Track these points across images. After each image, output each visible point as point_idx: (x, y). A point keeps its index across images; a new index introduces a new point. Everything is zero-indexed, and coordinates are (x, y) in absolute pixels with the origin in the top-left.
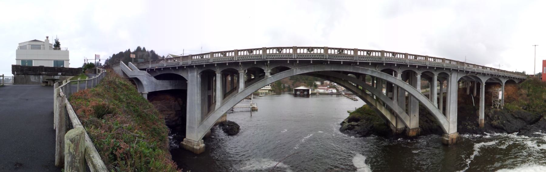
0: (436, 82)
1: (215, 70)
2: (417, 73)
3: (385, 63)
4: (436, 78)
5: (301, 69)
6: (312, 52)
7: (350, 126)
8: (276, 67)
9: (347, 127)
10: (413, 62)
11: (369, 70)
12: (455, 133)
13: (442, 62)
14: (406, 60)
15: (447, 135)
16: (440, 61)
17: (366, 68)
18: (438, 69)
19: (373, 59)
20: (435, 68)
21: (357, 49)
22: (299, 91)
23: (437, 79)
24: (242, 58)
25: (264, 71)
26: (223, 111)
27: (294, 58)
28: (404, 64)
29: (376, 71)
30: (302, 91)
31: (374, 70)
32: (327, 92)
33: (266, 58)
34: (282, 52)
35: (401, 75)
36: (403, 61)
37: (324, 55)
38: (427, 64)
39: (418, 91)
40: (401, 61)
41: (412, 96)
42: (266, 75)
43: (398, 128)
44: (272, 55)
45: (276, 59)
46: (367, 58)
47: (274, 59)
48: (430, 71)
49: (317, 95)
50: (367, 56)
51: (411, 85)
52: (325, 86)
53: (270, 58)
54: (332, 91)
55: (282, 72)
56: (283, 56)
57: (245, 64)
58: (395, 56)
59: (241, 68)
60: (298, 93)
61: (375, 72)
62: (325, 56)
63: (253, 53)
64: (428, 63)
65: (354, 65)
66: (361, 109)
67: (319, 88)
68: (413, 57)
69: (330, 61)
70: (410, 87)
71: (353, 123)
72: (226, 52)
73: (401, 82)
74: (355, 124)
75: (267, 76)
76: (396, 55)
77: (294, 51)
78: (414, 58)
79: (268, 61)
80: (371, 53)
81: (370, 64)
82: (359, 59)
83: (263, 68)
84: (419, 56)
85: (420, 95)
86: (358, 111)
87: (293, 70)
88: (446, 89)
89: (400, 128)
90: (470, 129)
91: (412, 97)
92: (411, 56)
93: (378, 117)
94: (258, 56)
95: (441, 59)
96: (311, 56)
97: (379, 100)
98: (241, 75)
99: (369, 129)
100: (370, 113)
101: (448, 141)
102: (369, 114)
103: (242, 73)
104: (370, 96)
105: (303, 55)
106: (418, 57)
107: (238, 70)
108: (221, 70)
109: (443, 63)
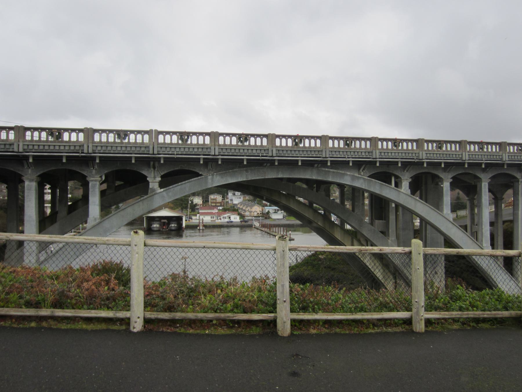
0: (486, 196)
1: (20, 173)
2: (441, 178)
3: (380, 162)
4: (485, 186)
6: (247, 144)
10: (435, 155)
11: (347, 175)
14: (421, 153)
16: (494, 150)
17: (341, 172)
18: (489, 166)
19: (356, 153)
20: (483, 166)
22: (157, 221)
23: (487, 190)
24: (104, 148)
25: (148, 179)
27: (325, 156)
28: (417, 160)
29: (360, 176)
30: (166, 221)
32: (220, 221)
33: (219, 152)
34: (189, 142)
35: (408, 183)
36: (414, 155)
37: (268, 150)
38: (464, 159)
39: (446, 216)
40: (410, 155)
41: (428, 225)
44: (171, 148)
45: (177, 154)
46: (345, 153)
47: (174, 154)
48: (471, 172)
49: (199, 230)
50: (237, 145)
51: (426, 202)
53: (166, 152)
54: (230, 218)
56: (191, 150)
57: (105, 161)
58: (399, 146)
59: (94, 171)
60: (155, 226)
61: (358, 178)
62: (270, 150)
63: (129, 139)
66: (313, 258)
68: (435, 145)
69: (279, 160)
70: (428, 208)
73: (410, 198)
75: (153, 190)
76: (400, 144)
78: (436, 146)
79: (96, 156)
80: (352, 142)
81: (351, 164)
82: (331, 156)
83: (145, 173)
84: (446, 142)
85: (450, 225)
86: (308, 263)
88: (512, 211)
91: (428, 227)
93: (352, 275)
94: (141, 147)
95: (496, 144)
96: (246, 151)
97: (359, 236)
98: (94, 186)
103: (96, 181)
105: (231, 149)
106: (444, 145)
107: (85, 173)
108: (39, 174)
109: (500, 154)
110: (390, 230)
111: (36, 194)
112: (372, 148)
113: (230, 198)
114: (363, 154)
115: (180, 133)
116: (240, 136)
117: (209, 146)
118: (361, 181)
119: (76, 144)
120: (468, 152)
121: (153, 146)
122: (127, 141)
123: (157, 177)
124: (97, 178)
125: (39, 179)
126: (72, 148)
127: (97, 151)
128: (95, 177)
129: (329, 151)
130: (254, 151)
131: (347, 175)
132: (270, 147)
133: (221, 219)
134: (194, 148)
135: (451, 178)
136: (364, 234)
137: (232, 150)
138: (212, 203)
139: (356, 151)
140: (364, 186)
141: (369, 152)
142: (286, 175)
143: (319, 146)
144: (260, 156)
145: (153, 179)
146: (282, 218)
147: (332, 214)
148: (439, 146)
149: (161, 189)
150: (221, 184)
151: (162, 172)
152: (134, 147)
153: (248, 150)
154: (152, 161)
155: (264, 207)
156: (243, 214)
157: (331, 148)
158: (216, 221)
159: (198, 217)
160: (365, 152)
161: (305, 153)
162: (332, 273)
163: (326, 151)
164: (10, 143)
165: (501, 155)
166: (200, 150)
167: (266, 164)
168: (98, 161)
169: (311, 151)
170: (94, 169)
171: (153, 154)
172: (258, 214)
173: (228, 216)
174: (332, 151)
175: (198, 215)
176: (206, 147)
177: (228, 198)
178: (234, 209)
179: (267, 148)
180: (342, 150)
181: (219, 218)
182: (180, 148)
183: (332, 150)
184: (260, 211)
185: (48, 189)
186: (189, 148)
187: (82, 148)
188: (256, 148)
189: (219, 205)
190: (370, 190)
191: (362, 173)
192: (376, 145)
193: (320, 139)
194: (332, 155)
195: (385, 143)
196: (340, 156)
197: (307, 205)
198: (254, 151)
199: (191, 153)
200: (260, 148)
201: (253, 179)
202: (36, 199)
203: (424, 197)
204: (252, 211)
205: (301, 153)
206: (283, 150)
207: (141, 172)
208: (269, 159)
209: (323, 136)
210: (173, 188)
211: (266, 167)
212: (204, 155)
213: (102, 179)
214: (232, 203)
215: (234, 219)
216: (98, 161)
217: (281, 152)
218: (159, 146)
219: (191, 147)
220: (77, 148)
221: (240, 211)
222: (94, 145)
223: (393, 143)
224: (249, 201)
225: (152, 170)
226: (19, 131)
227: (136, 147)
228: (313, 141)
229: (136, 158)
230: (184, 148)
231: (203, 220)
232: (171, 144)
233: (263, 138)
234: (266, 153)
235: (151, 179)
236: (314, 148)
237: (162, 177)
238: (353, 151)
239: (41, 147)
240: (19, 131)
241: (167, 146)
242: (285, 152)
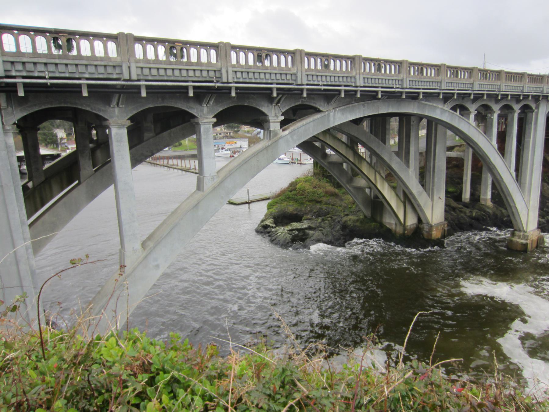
1: (101, 114)
7: (296, 232)
8: (293, 105)
9: (291, 234)
11: (438, 107)
12: (534, 230)
13: (290, 65)
15: (522, 233)
21: (229, 44)
26: (157, 266)
43: (408, 226)
47: (44, 78)
50: (168, 62)
72: (327, 57)
82: (235, 80)
83: (264, 109)
89: (410, 225)
90: (544, 223)
95: (347, 58)
100: (319, 200)
101: (526, 245)
102: (317, 202)
103: (209, 123)
104: (367, 162)
115: (169, 41)
116: (172, 45)
120: (306, 70)
122: (74, 53)
135: (214, 117)
139: (288, 72)
144: (215, 81)
148: (325, 64)
151: (283, 109)
162: (318, 206)
164: (115, 65)
165: (354, 77)
171: (130, 80)
192: (228, 58)
193: (115, 40)
195: (242, 55)
197: (343, 142)
203: (373, 132)
207: (260, 109)
211: (381, 100)
212: (277, 84)
223: (256, 54)
226: (127, 43)
228: (150, 48)
234: (117, 74)
240: (127, 43)
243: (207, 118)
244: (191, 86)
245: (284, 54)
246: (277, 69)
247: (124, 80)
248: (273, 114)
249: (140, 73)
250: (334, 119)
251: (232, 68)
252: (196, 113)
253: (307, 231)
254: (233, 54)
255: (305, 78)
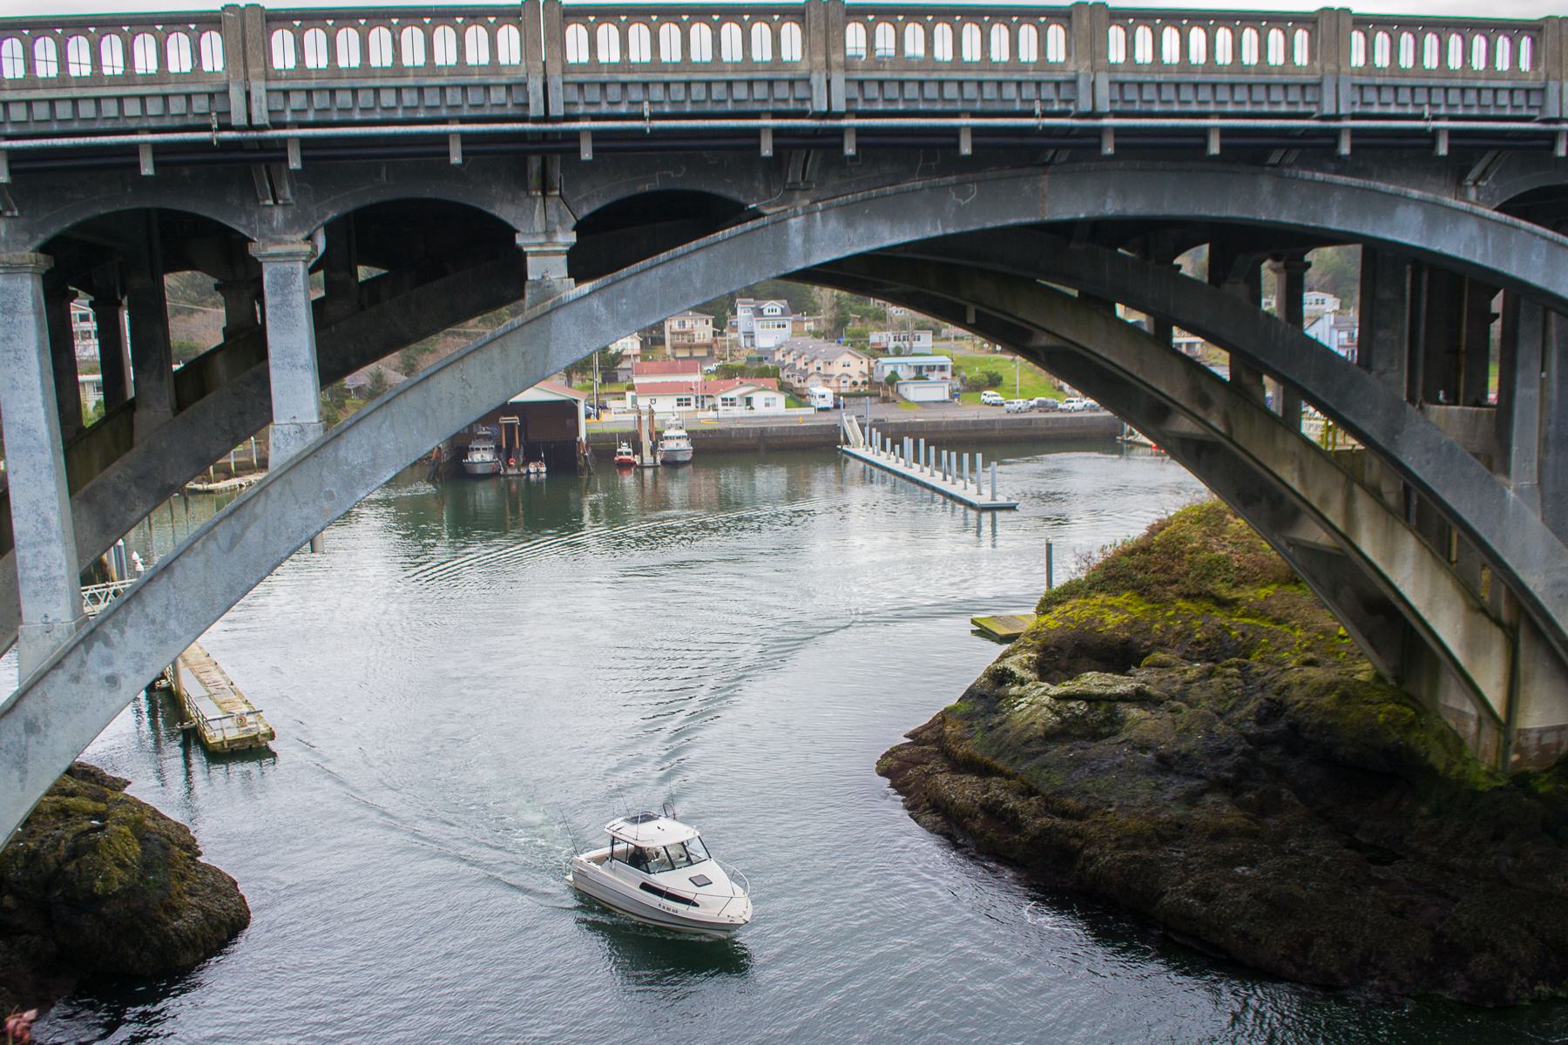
5: (850, 214)
7: (1081, 707)
9: (1057, 713)
11: (1407, 199)
13: (1525, 64)
19: (1471, 97)
21: (1347, 11)
24: (320, 101)
25: (519, 240)
29: (1463, 205)
31: (1449, 201)
33: (848, 101)
37: (1073, 82)
42: (532, 276)
44: (624, 85)
45: (654, 117)
46: (1421, 97)
47: (640, 117)
52: (690, 364)
53: (604, 108)
54: (749, 401)
55: (680, 250)
59: (278, 215)
60: (476, 457)
62: (1082, 84)
64: (1104, 92)
65: (1292, 157)
66: (1140, 558)
67: (637, 380)
71: (1093, 681)
74: (1120, 689)
77: (818, 39)
79: (285, 140)
83: (505, 212)
87: (780, 222)
89: (1543, 732)
92: (1197, 36)
93: (1304, 627)
94: (487, 87)
98: (286, 281)
99: (1252, 728)
105: (902, 83)
107: (239, 225)
108: (41, 239)
110: (1514, 449)
111: (40, 328)
112: (1541, 69)
113: (742, 328)
114: (1503, 99)
117: (802, 71)
118: (1470, 228)
119: (192, 88)
121: (545, 77)
123: (558, 228)
124: (293, 242)
125: (45, 262)
126: (177, 106)
127: (289, 117)
128: (286, 243)
129: (1353, 85)
130: (1010, 92)
131: (1407, 199)
132: (1081, 71)
133: (715, 408)
134: (730, 83)
136: (1407, 464)
137: (908, 87)
138: (674, 347)
139: (1471, 83)
140: (1479, 252)
141: (1528, 91)
142: (1136, 206)
143: (1305, 63)
144: (647, 114)
145: (542, 239)
146: (947, 397)
147: (1266, 379)
149: (579, 281)
150: (849, 252)
152: (456, 86)
153: (980, 83)
154: (535, 152)
155: (874, 357)
156: (798, 385)
157: (1360, 72)
158: (700, 415)
159: (628, 403)
160: (1512, 91)
161: (1241, 94)
163: (1337, 86)
166: (760, 91)
167: (1051, 153)
168: (295, 164)
169: (1268, 86)
170: (276, 202)
171: (547, 118)
172: (855, 384)
173: (741, 396)
174: (1361, 87)
175: (629, 394)
176: (786, 75)
177: (735, 328)
178: (761, 369)
179: (1070, 75)
180: (1408, 82)
181: (708, 402)
182: (667, 84)
183: (1364, 80)
184: (864, 375)
185: (80, 307)
186: (709, 84)
187: (219, 105)
188: (1017, 77)
189: (703, 353)
190: (1506, 271)
191: (1472, 194)
192: (1097, 47)
193: (1310, 26)
194: (1363, 104)
196: (1400, 110)
198: (1010, 92)
199: (719, 108)
200: (1038, 76)
201: (989, 225)
202: (40, 351)
204: (831, 376)
205: (1223, 94)
206: (1140, 85)
208: (1071, 128)
209: (1323, 11)
210: (634, 278)
211: (1050, 169)
212: (776, 115)
213: (315, 248)
214: (753, 345)
215: (767, 405)
216: (295, 164)
217: (1131, 94)
218: (569, 78)
219: (720, 77)
220: (200, 105)
221: (783, 375)
222: (274, 85)
224: (816, 335)
225: (534, 198)
227: (464, 88)
228: (971, 33)
229: (466, 138)
230: (688, 84)
231: (652, 413)
232: (625, 65)
233: (1047, 25)
235: (532, 241)
236: (1281, 70)
237: (579, 228)
238: (1459, 83)
239: (41, 112)
241: (605, 77)
242: (1150, 93)
243: (279, 242)
244: (1215, 127)
245: (1463, 31)
246: (1531, 77)
247: (536, 120)
248: (539, 225)
249: (1117, 97)
250: (808, 239)
251: (1109, 72)
252: (245, 227)
253: (1121, 706)
254: (1357, 39)
255: (1346, 93)
